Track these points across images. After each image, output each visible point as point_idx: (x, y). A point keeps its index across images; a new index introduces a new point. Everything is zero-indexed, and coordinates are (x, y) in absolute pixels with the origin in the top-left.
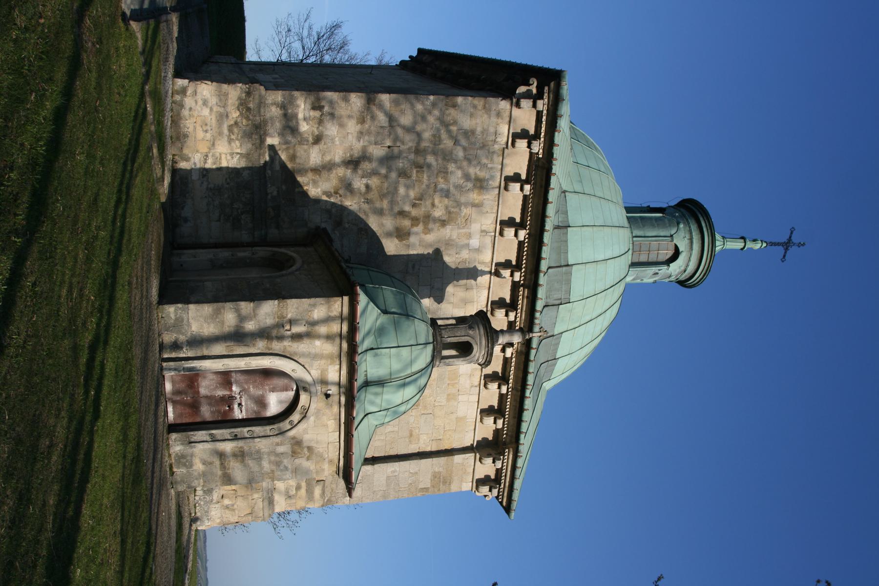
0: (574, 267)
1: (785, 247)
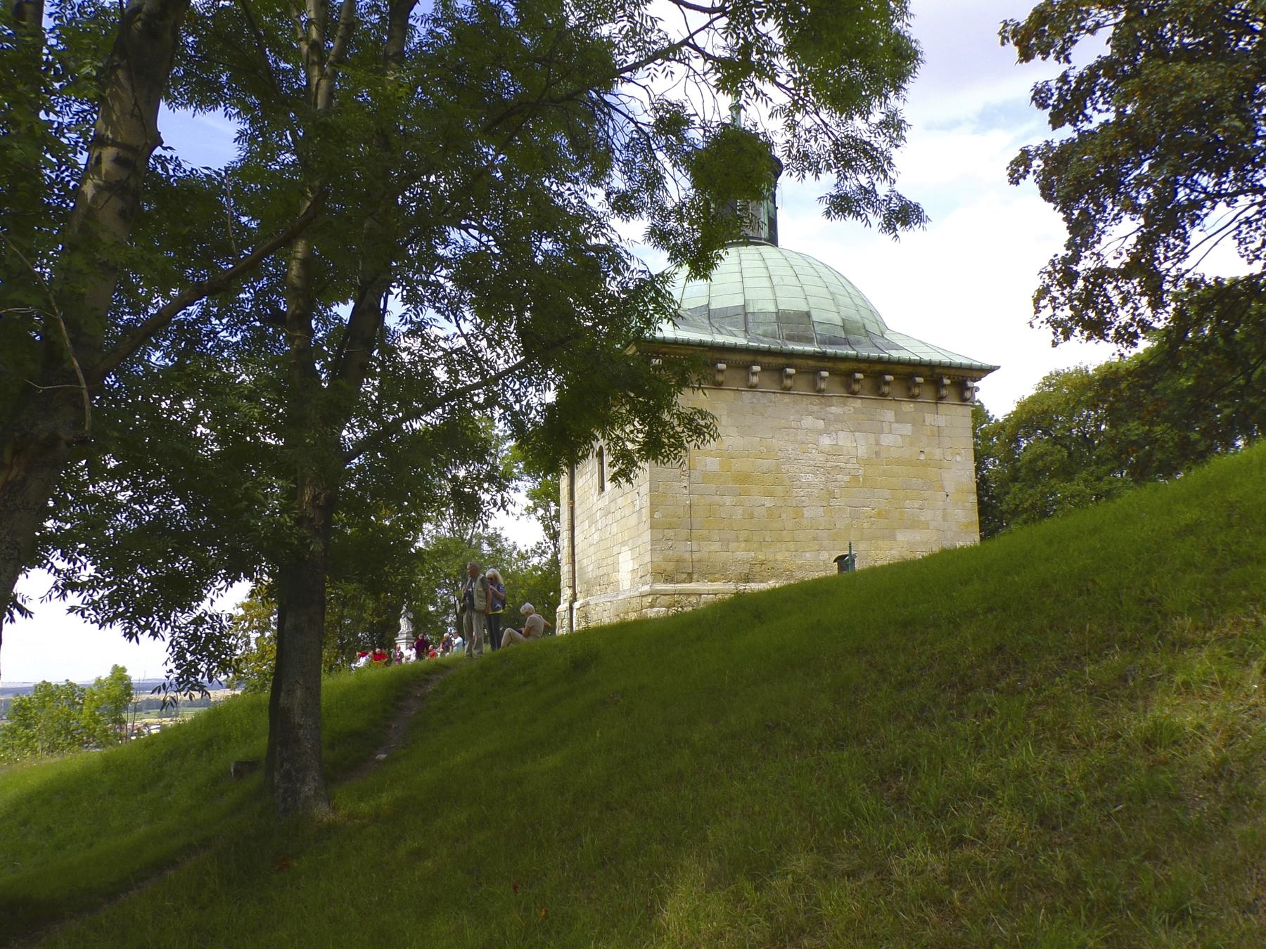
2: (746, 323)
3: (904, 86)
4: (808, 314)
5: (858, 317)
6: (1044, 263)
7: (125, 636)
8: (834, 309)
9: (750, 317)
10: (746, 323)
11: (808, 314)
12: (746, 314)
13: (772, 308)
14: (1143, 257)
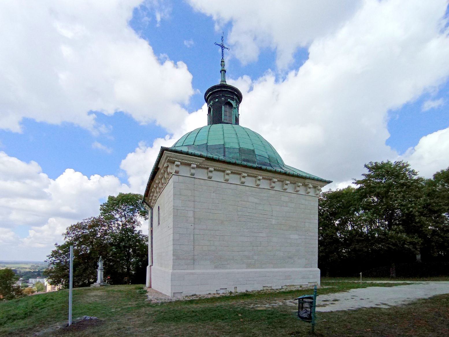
1: (223, 48)
2: (224, 152)
3: (367, 171)
4: (253, 151)
5: (275, 157)
6: (374, 161)
7: (101, 205)
8: (264, 150)
9: (226, 150)
10: (224, 152)
11: (253, 151)
12: (225, 148)
13: (237, 147)
14: (330, 212)
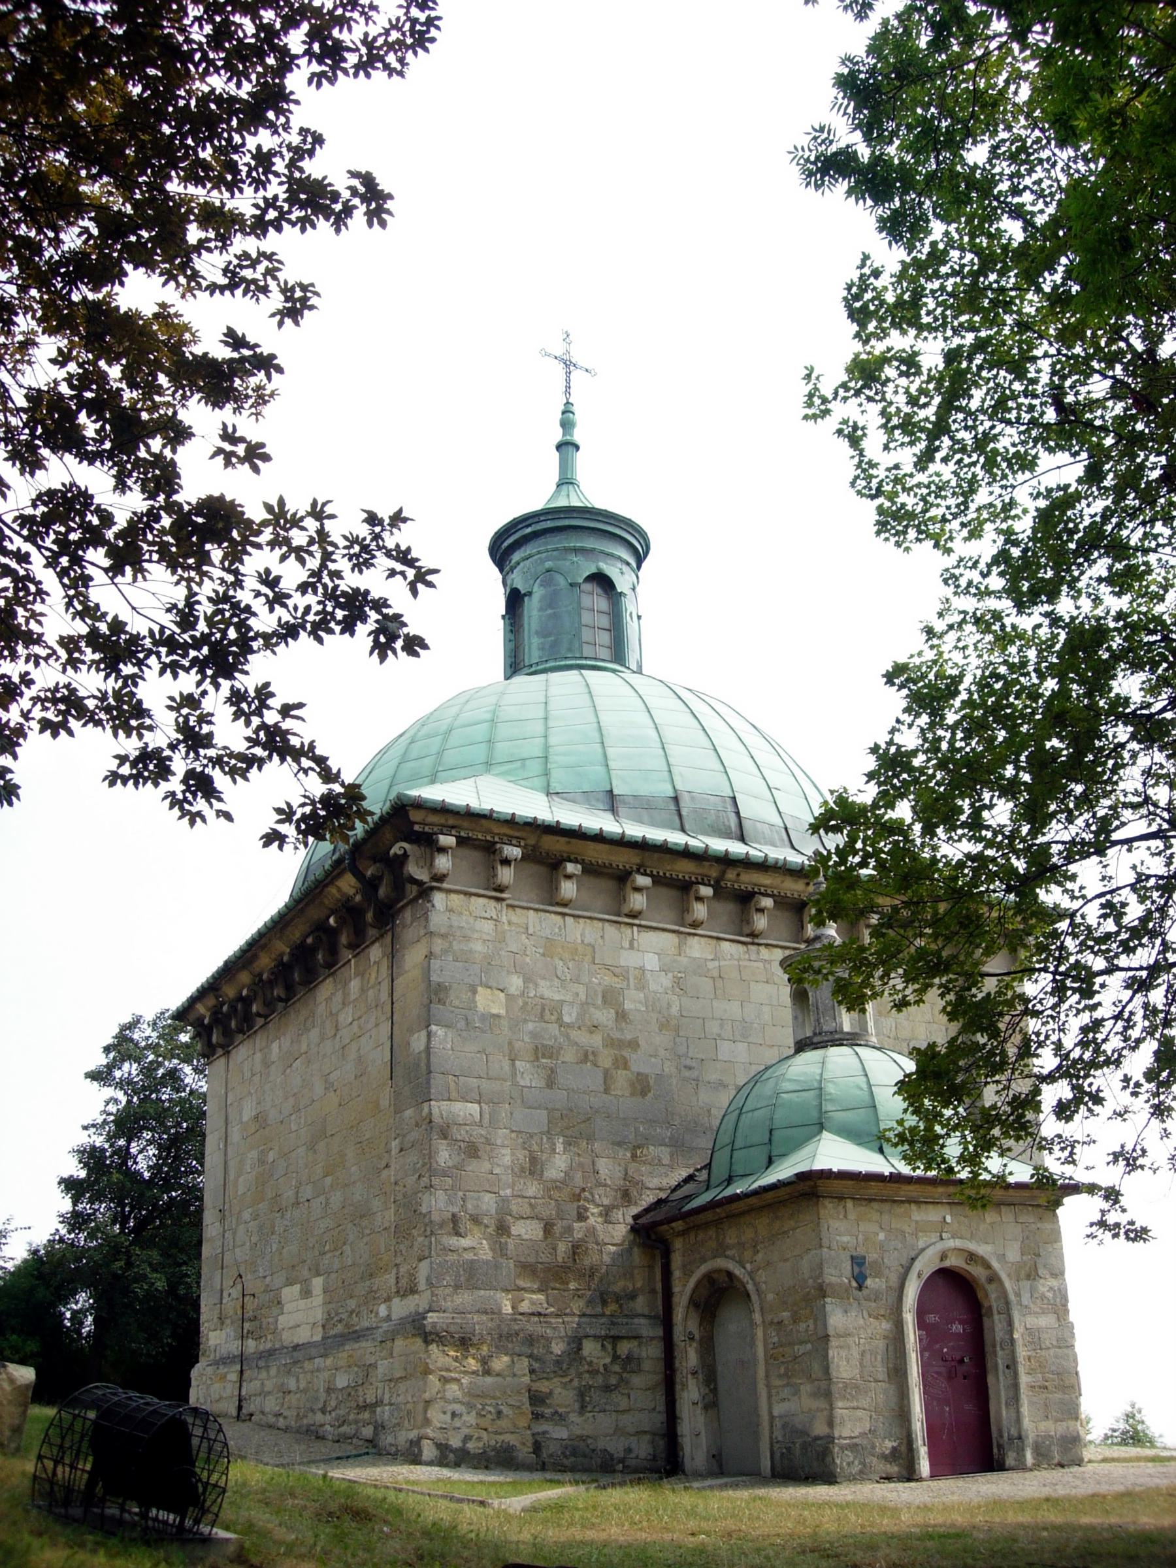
0: (679, 786)
